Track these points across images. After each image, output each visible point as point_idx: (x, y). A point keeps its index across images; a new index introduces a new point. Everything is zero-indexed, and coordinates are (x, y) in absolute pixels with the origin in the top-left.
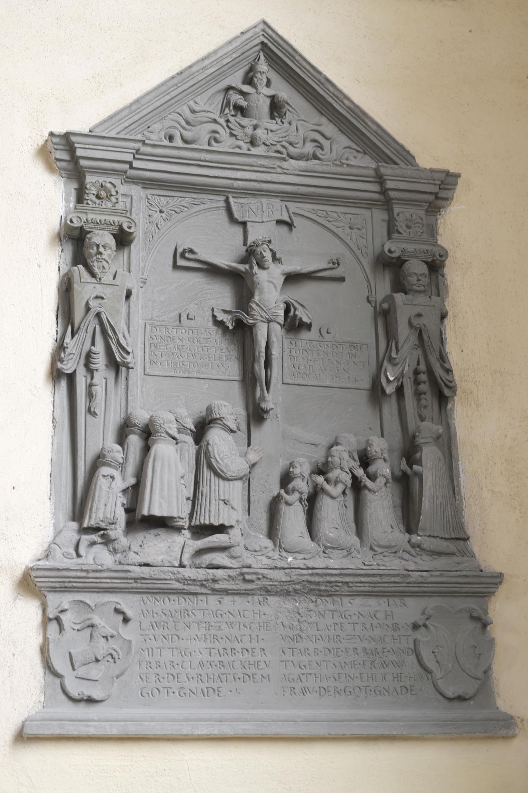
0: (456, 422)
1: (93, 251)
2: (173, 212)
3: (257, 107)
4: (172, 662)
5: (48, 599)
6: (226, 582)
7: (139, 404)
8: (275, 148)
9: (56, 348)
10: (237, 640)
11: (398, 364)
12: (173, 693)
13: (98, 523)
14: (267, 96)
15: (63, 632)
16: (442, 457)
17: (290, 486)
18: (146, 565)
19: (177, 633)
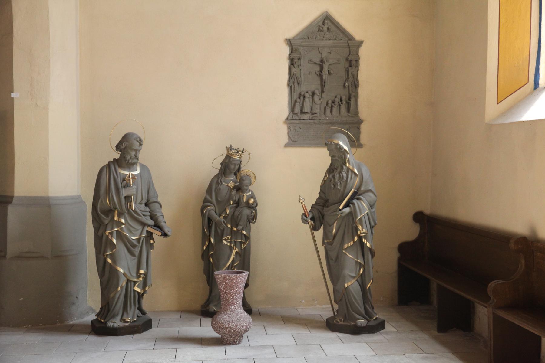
17: (328, 105)
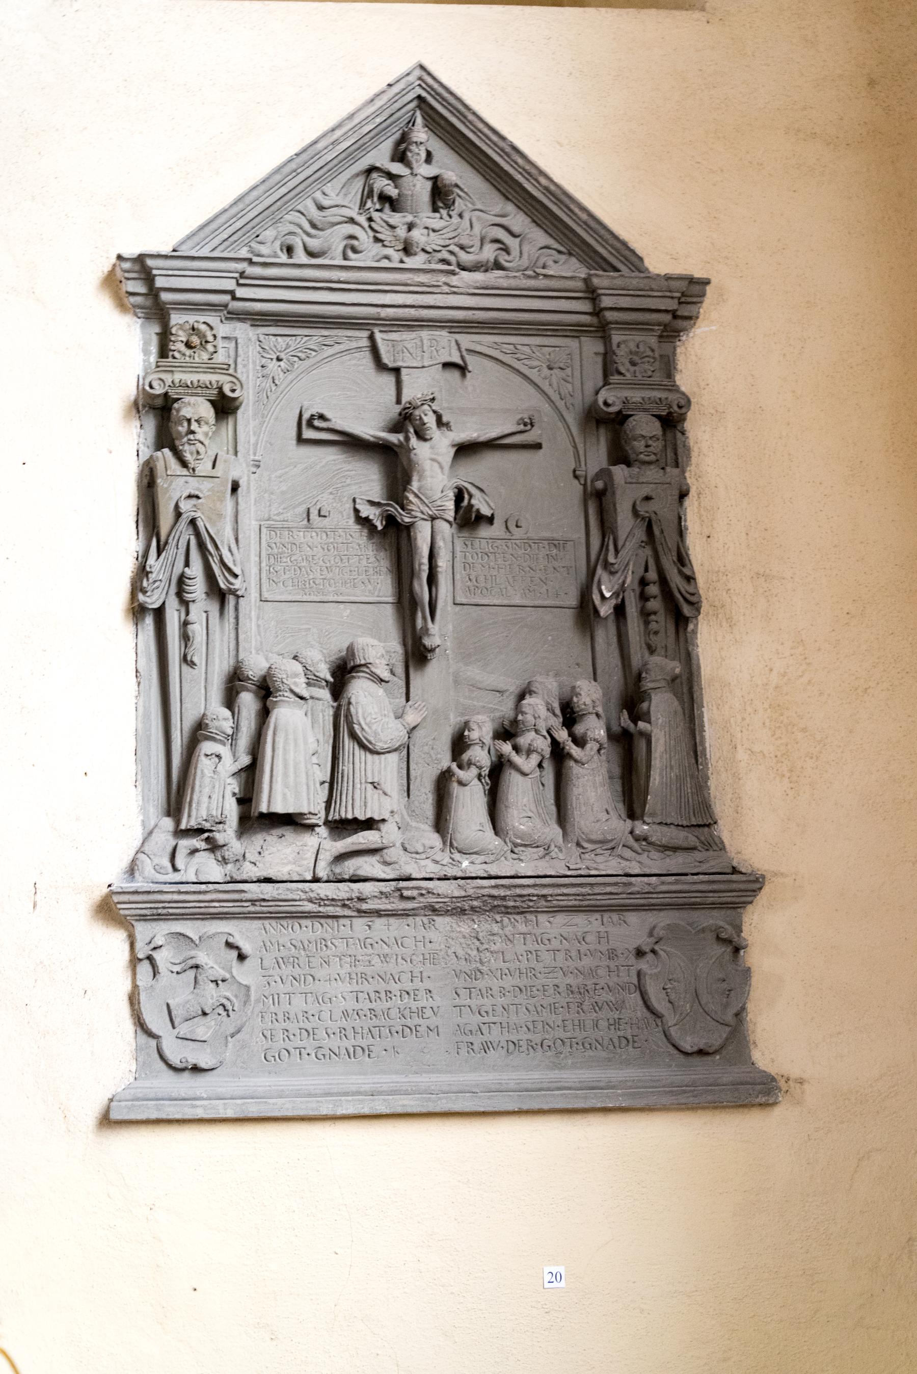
0: (700, 650)
1: (183, 429)
2: (296, 359)
3: (412, 195)
4: (306, 1012)
5: (136, 932)
6: (377, 901)
7: (253, 643)
8: (439, 256)
9: (138, 569)
10: (394, 979)
11: (617, 572)
12: (308, 1054)
13: (199, 824)
14: (428, 179)
15: (157, 976)
16: (679, 709)
17: (465, 757)
18: (268, 880)
19: (312, 972)
